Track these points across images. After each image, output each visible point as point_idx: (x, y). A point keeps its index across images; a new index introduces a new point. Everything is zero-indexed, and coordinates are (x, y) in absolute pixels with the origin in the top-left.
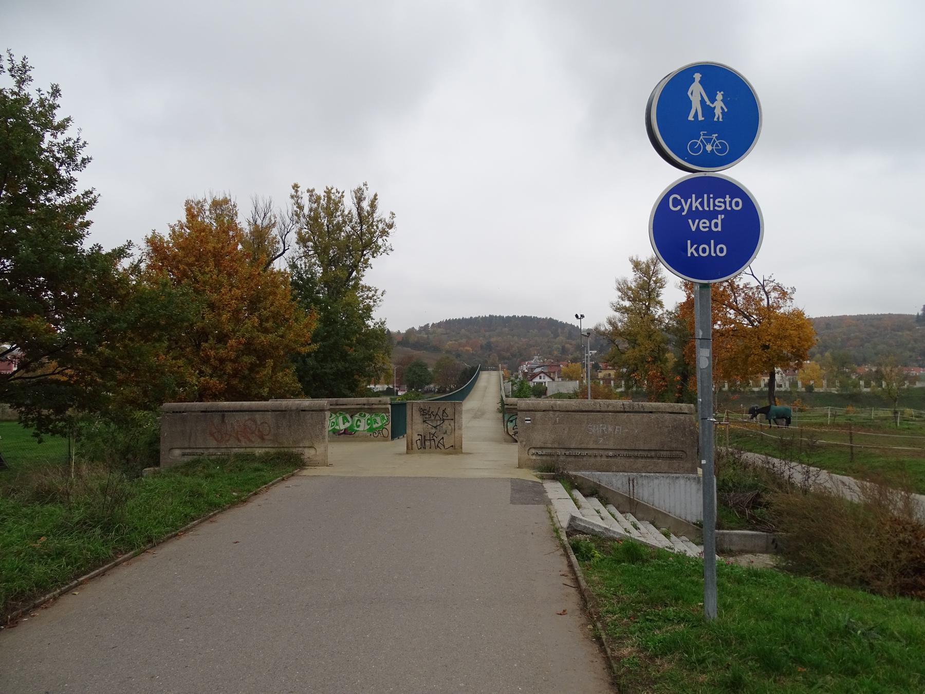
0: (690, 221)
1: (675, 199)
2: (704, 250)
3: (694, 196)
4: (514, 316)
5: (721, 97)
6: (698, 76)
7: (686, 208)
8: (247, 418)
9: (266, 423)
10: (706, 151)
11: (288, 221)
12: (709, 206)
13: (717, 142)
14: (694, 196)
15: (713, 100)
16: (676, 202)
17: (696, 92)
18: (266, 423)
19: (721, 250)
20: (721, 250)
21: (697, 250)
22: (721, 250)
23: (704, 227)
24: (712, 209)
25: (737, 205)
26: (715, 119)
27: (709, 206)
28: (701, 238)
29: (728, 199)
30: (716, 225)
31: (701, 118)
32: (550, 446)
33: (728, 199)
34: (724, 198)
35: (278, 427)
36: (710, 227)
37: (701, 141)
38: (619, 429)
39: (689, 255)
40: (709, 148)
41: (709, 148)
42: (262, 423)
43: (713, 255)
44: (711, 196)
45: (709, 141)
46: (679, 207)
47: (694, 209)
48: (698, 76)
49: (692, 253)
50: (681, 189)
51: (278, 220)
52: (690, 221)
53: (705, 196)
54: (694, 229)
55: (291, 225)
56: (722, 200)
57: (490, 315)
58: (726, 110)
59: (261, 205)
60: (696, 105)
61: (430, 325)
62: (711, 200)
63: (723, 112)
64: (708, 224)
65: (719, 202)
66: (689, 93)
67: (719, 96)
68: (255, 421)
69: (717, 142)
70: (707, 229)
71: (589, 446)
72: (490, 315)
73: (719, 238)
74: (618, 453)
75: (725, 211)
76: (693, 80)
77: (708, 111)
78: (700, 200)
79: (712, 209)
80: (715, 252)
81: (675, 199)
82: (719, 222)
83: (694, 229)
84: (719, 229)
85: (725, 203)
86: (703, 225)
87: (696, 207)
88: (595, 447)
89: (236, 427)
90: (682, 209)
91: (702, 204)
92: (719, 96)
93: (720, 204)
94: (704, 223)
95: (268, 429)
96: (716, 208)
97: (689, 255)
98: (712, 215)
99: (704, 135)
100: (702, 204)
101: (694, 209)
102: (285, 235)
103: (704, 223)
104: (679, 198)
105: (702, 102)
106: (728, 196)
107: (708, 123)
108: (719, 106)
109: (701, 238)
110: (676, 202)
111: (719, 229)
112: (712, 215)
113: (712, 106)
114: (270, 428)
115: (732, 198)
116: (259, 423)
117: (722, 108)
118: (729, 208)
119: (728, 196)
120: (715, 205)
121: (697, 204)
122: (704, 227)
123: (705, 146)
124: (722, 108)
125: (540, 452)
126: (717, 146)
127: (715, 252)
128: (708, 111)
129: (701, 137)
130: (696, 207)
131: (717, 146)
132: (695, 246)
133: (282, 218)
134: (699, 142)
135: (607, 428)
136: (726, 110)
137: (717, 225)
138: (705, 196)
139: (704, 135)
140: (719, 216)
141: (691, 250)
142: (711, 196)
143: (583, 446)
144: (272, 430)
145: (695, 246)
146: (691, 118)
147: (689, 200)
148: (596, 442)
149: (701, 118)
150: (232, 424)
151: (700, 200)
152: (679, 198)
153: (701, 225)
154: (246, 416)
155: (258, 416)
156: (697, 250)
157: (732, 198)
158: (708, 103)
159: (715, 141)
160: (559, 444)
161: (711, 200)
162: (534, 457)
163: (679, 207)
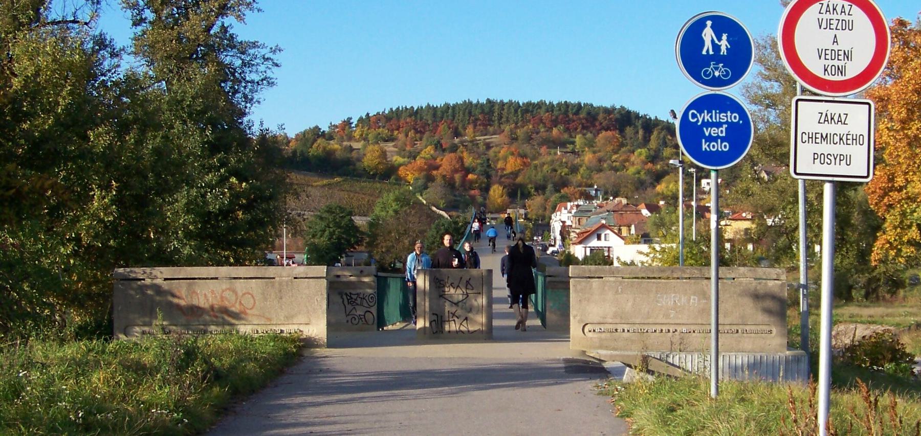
0: (705, 129)
1: (693, 114)
2: (714, 146)
3: (706, 111)
4: (447, 106)
5: (726, 38)
6: (709, 23)
7: (701, 120)
8: (224, 287)
9: (249, 294)
10: (714, 75)
12: (716, 119)
13: (723, 69)
14: (706, 111)
16: (694, 116)
17: (708, 34)
18: (249, 294)
19: (725, 147)
20: (725, 146)
21: (709, 146)
22: (725, 146)
23: (714, 133)
24: (718, 120)
25: (735, 118)
26: (722, 54)
27: (716, 119)
28: (711, 139)
29: (729, 114)
30: (722, 132)
33: (729, 114)
34: (726, 113)
35: (265, 299)
36: (718, 133)
37: (712, 69)
38: (694, 299)
39: (704, 150)
40: (717, 74)
41: (717, 74)
42: (244, 294)
43: (720, 150)
44: (718, 111)
45: (716, 69)
46: (696, 119)
47: (706, 120)
48: (709, 23)
49: (705, 148)
50: (700, 104)
52: (705, 129)
53: (714, 112)
54: (707, 134)
56: (725, 115)
58: (729, 47)
60: (708, 44)
62: (718, 115)
63: (727, 49)
64: (717, 131)
65: (723, 116)
66: (703, 35)
67: (724, 37)
68: (234, 292)
69: (723, 69)
70: (716, 135)
72: (489, 101)
73: (723, 140)
74: (693, 328)
75: (727, 122)
77: (716, 48)
78: (710, 114)
79: (718, 120)
80: (721, 148)
81: (693, 114)
82: (724, 129)
83: (707, 134)
84: (724, 135)
85: (727, 116)
86: (714, 131)
87: (708, 120)
88: (666, 322)
89: (210, 299)
90: (698, 121)
91: (711, 117)
92: (724, 37)
93: (724, 117)
94: (714, 130)
95: (252, 301)
96: (721, 120)
97: (704, 150)
98: (718, 125)
99: (713, 64)
100: (711, 117)
101: (706, 120)
103: (714, 130)
104: (695, 112)
105: (713, 41)
106: (729, 112)
107: (716, 57)
108: (724, 44)
109: (711, 139)
110: (694, 116)
111: (724, 135)
112: (718, 125)
113: (719, 44)
114: (255, 301)
115: (732, 113)
116: (240, 294)
117: (726, 45)
118: (730, 121)
119: (729, 112)
120: (720, 118)
121: (706, 146)
122: (714, 133)
123: (714, 72)
124: (726, 45)
125: (597, 328)
126: (722, 72)
127: (721, 148)
128: (716, 48)
129: (712, 66)
130: (708, 120)
131: (722, 72)
132: (708, 143)
134: (710, 69)
135: (680, 298)
136: (729, 47)
137: (722, 131)
138: (714, 112)
139: (713, 64)
140: (724, 126)
141: (705, 146)
142: (718, 111)
143: (651, 321)
144: (257, 303)
145: (708, 143)
146: (704, 52)
147: (703, 115)
149: (711, 52)
150: (205, 295)
151: (710, 114)
152: (695, 112)
153: (712, 132)
156: (709, 146)
157: (732, 113)
158: (717, 42)
159: (721, 69)
160: (621, 318)
161: (718, 115)
162: (590, 335)
163: (696, 119)
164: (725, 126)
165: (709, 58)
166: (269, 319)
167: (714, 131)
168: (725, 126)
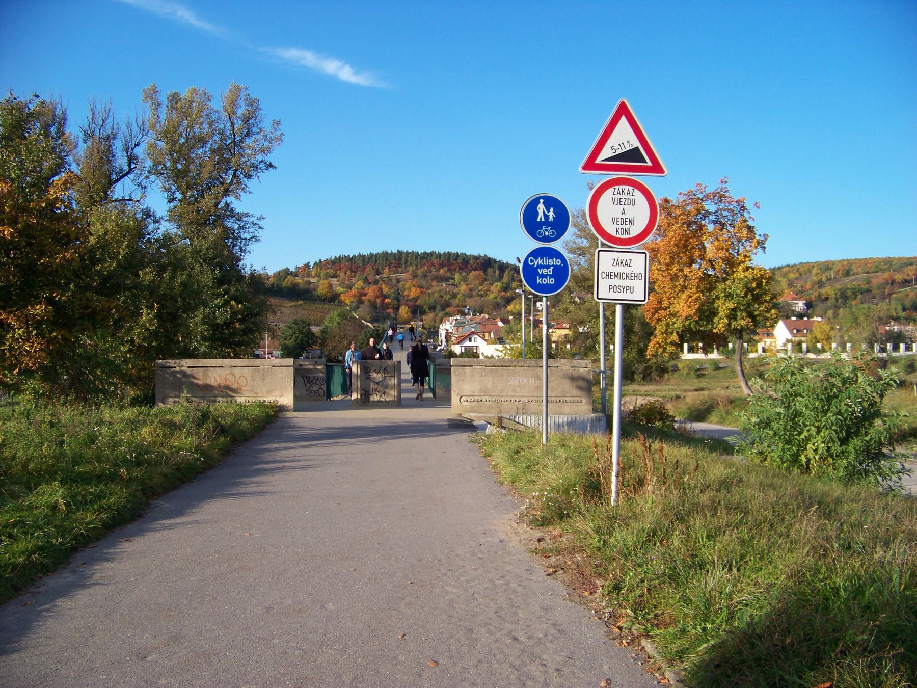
6: (542, 201)
11: (135, 130)
15: (548, 211)
16: (532, 261)
17: (541, 208)
19: (552, 281)
25: (558, 262)
28: (542, 276)
29: (554, 260)
31: (543, 220)
32: (478, 394)
33: (554, 260)
35: (254, 380)
40: (547, 234)
45: (546, 230)
48: (542, 201)
50: (536, 254)
51: (124, 128)
55: (141, 135)
57: (399, 251)
59: (99, 108)
60: (541, 214)
61: (312, 264)
67: (552, 210)
68: (234, 375)
71: (508, 394)
72: (399, 251)
73: (551, 276)
74: (531, 399)
75: (553, 265)
76: (539, 203)
77: (546, 217)
86: (545, 271)
88: (514, 394)
92: (552, 210)
93: (551, 262)
98: (548, 267)
102: (132, 150)
105: (544, 212)
107: (546, 223)
108: (551, 214)
109: (542, 276)
110: (532, 261)
112: (548, 267)
116: (237, 376)
125: (469, 399)
128: (546, 217)
133: (129, 126)
137: (550, 271)
141: (539, 281)
143: (504, 394)
146: (538, 220)
148: (514, 391)
149: (543, 220)
154: (227, 371)
155: (237, 370)
162: (465, 403)
164: (552, 268)
165: (541, 224)
166: (257, 393)
167: (545, 271)
168: (552, 268)
